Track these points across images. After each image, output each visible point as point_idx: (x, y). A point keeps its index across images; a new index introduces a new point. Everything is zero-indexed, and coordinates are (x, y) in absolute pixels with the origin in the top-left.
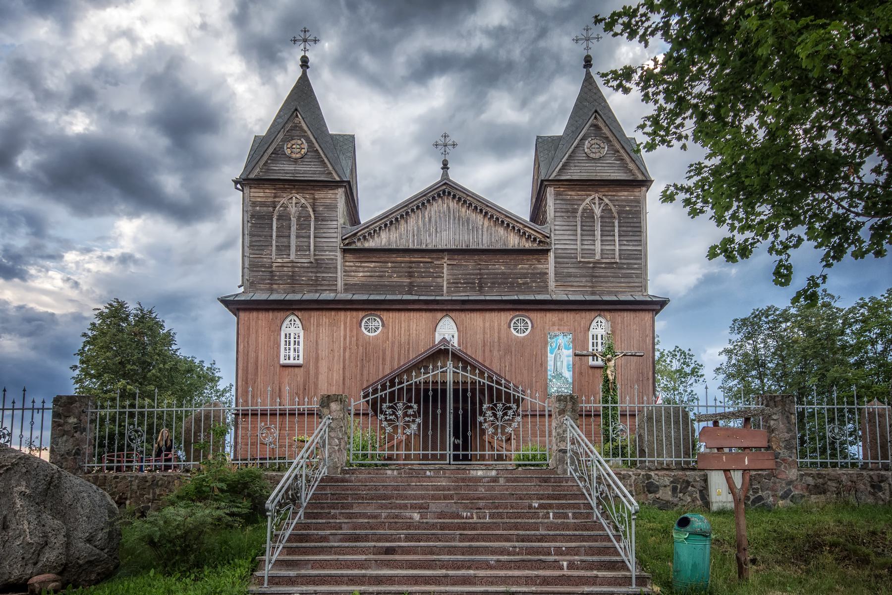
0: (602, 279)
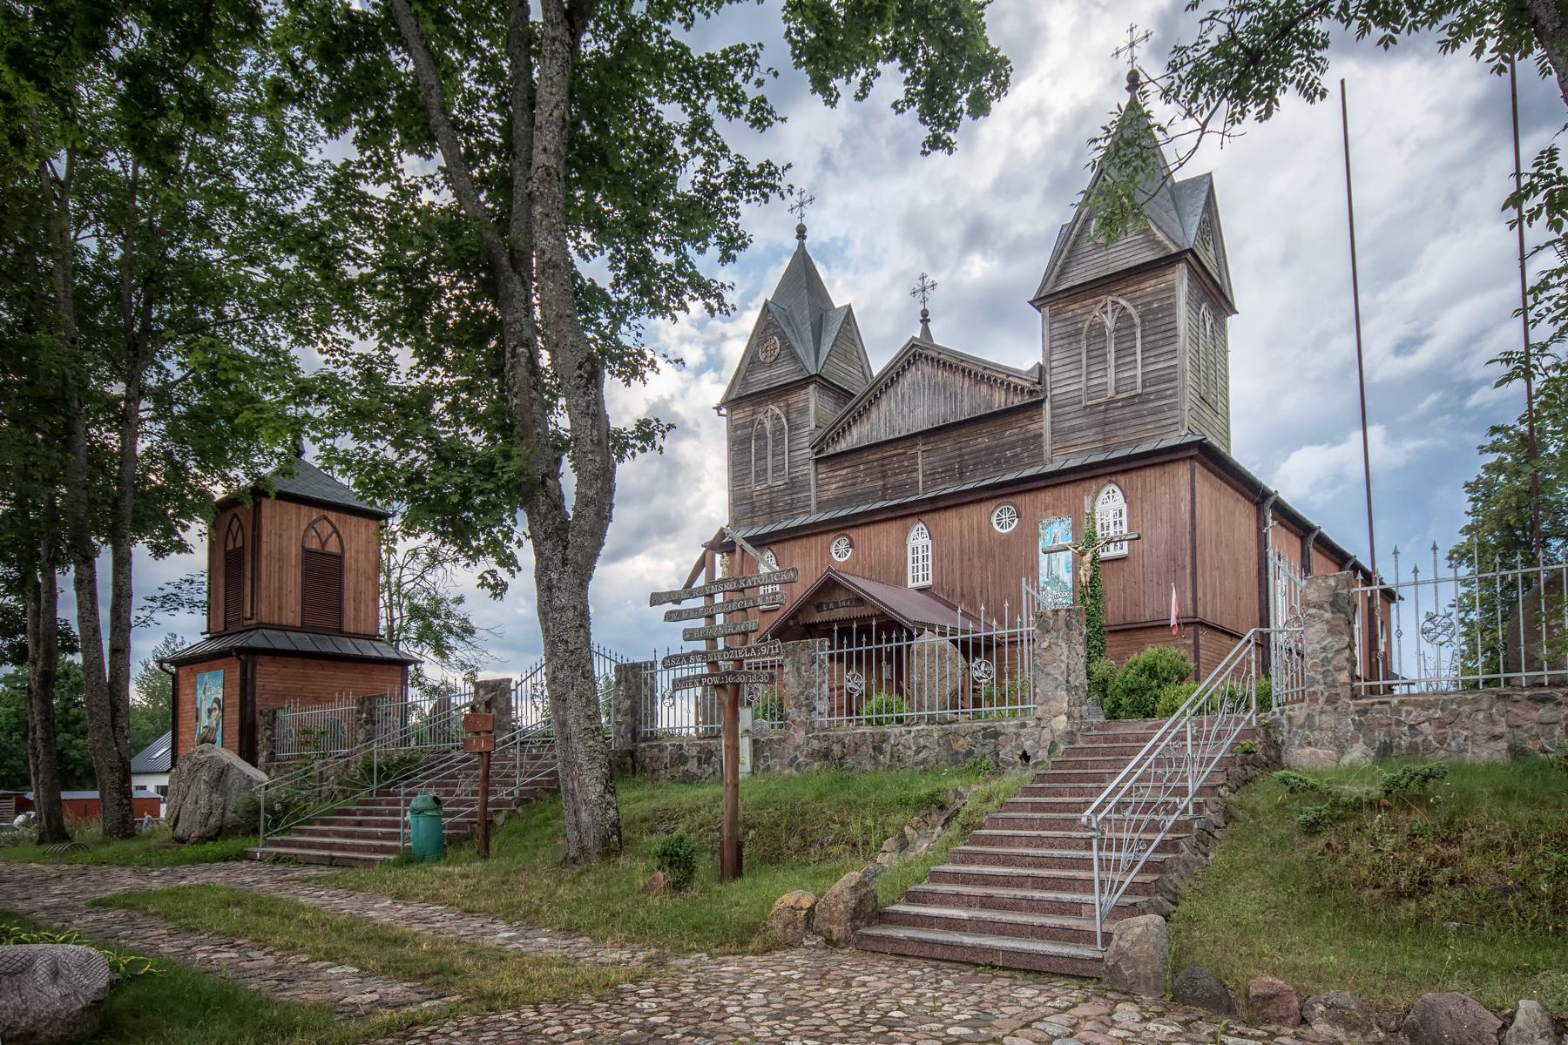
0: (1118, 425)
